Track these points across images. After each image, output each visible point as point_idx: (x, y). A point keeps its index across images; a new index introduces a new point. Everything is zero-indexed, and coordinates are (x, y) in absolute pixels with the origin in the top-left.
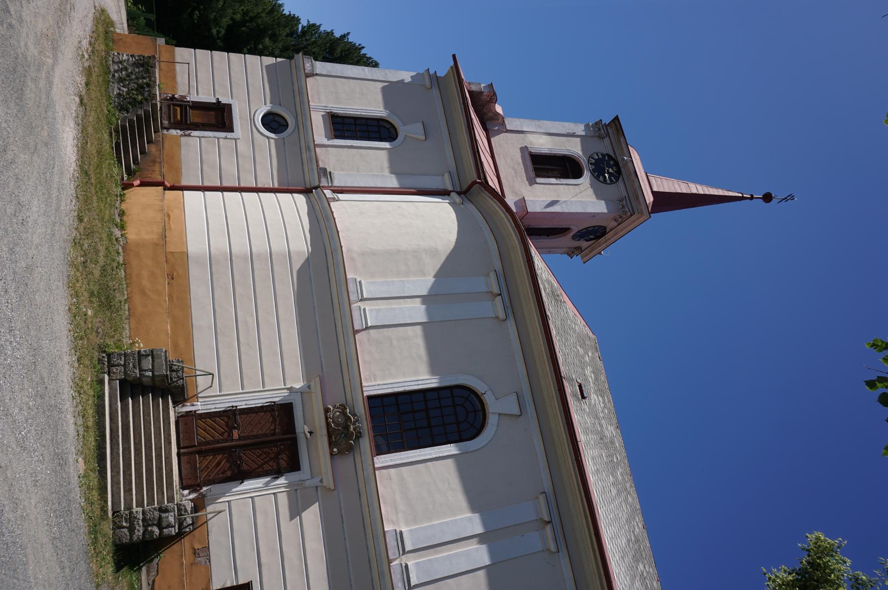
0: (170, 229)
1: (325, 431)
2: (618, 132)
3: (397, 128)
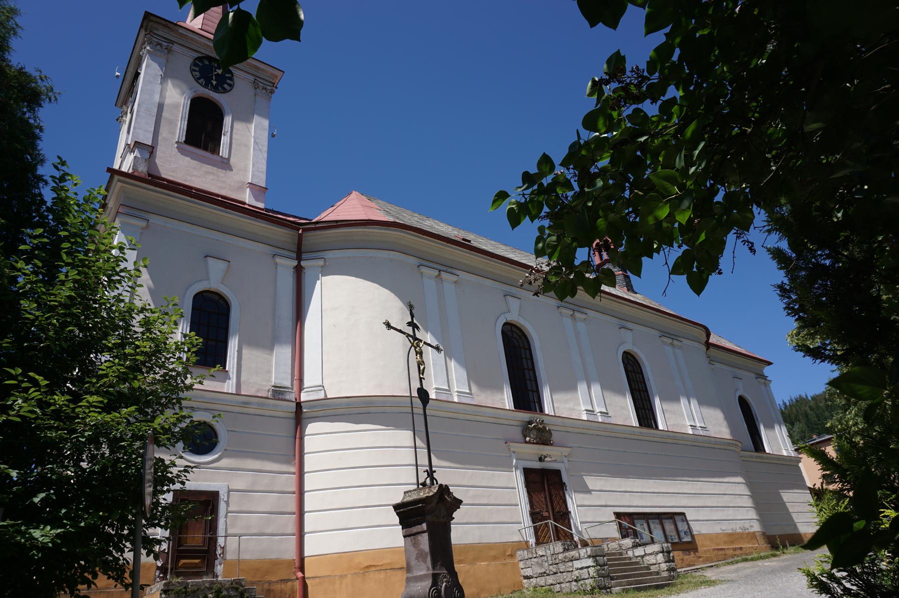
0: (390, 564)
1: (542, 447)
2: (169, 27)
3: (207, 289)
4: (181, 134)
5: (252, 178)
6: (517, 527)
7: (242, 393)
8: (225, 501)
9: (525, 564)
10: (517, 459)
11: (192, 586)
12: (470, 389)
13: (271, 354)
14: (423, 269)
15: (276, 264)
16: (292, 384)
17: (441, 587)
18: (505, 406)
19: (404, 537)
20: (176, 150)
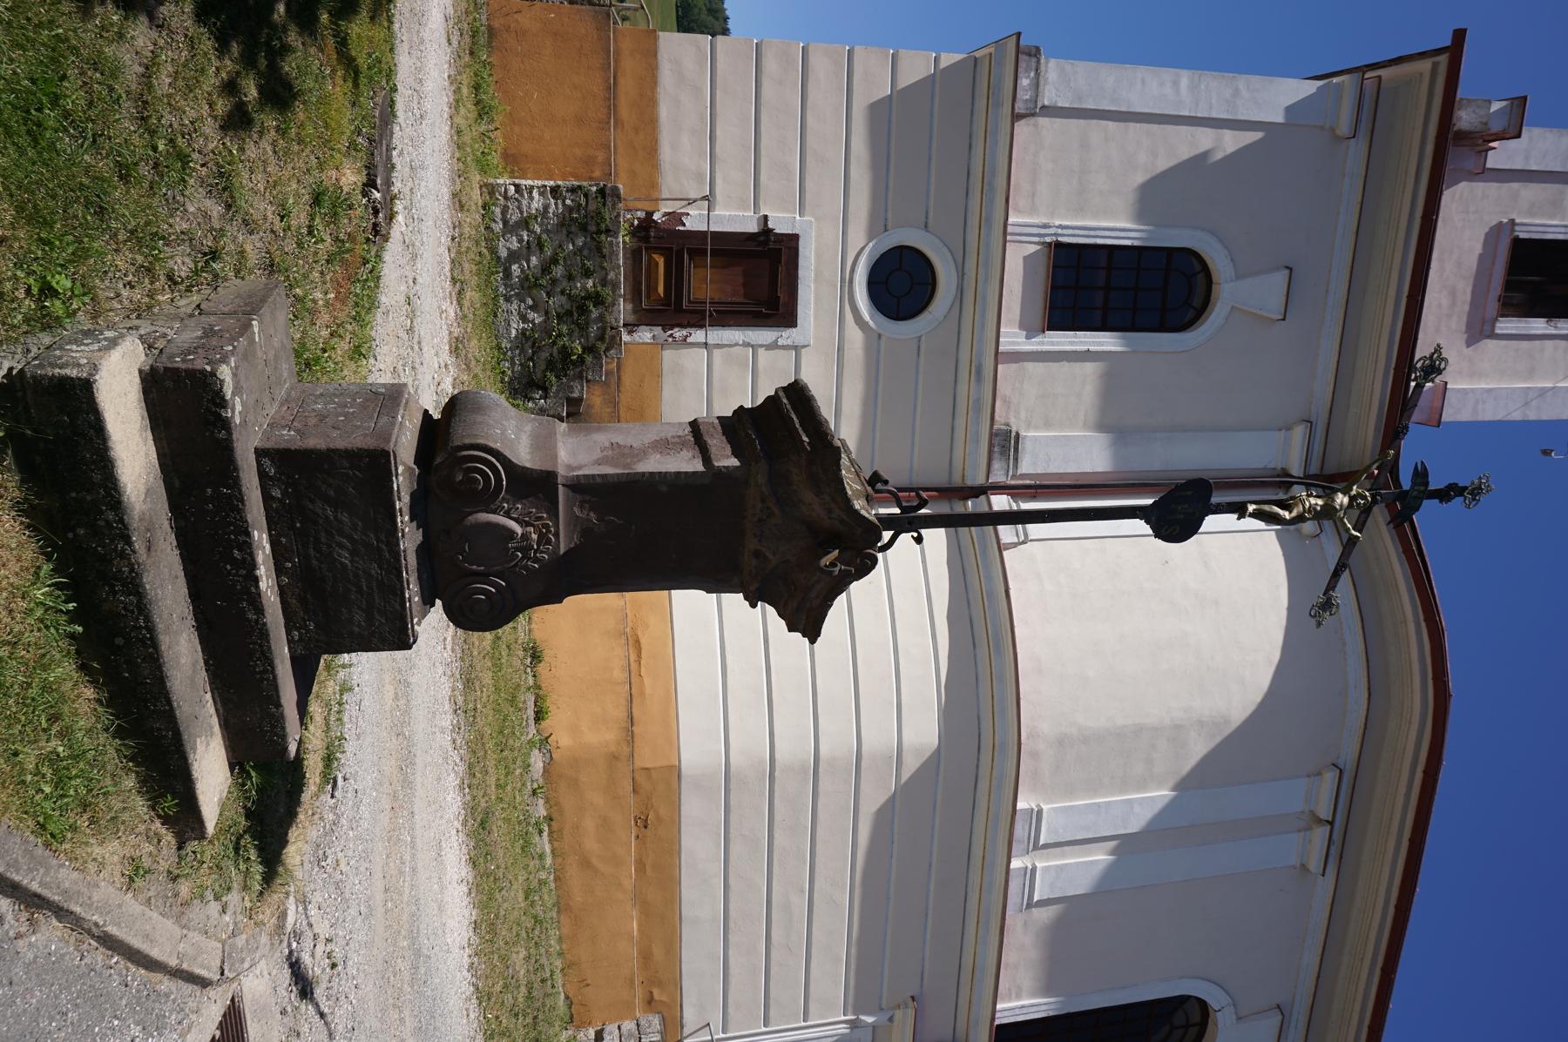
0: (642, 693)
3: (1215, 278)
4: (1533, 229)
5: (1459, 390)
6: (716, 1021)
7: (1000, 367)
8: (776, 341)
9: (630, 1035)
10: (874, 1027)
11: (611, 243)
12: (1042, 903)
13: (1086, 427)
14: (1330, 777)
15: (1289, 428)
16: (1023, 476)
17: (508, 515)
18: (1003, 1001)
19: (694, 424)
20: (1494, 223)
